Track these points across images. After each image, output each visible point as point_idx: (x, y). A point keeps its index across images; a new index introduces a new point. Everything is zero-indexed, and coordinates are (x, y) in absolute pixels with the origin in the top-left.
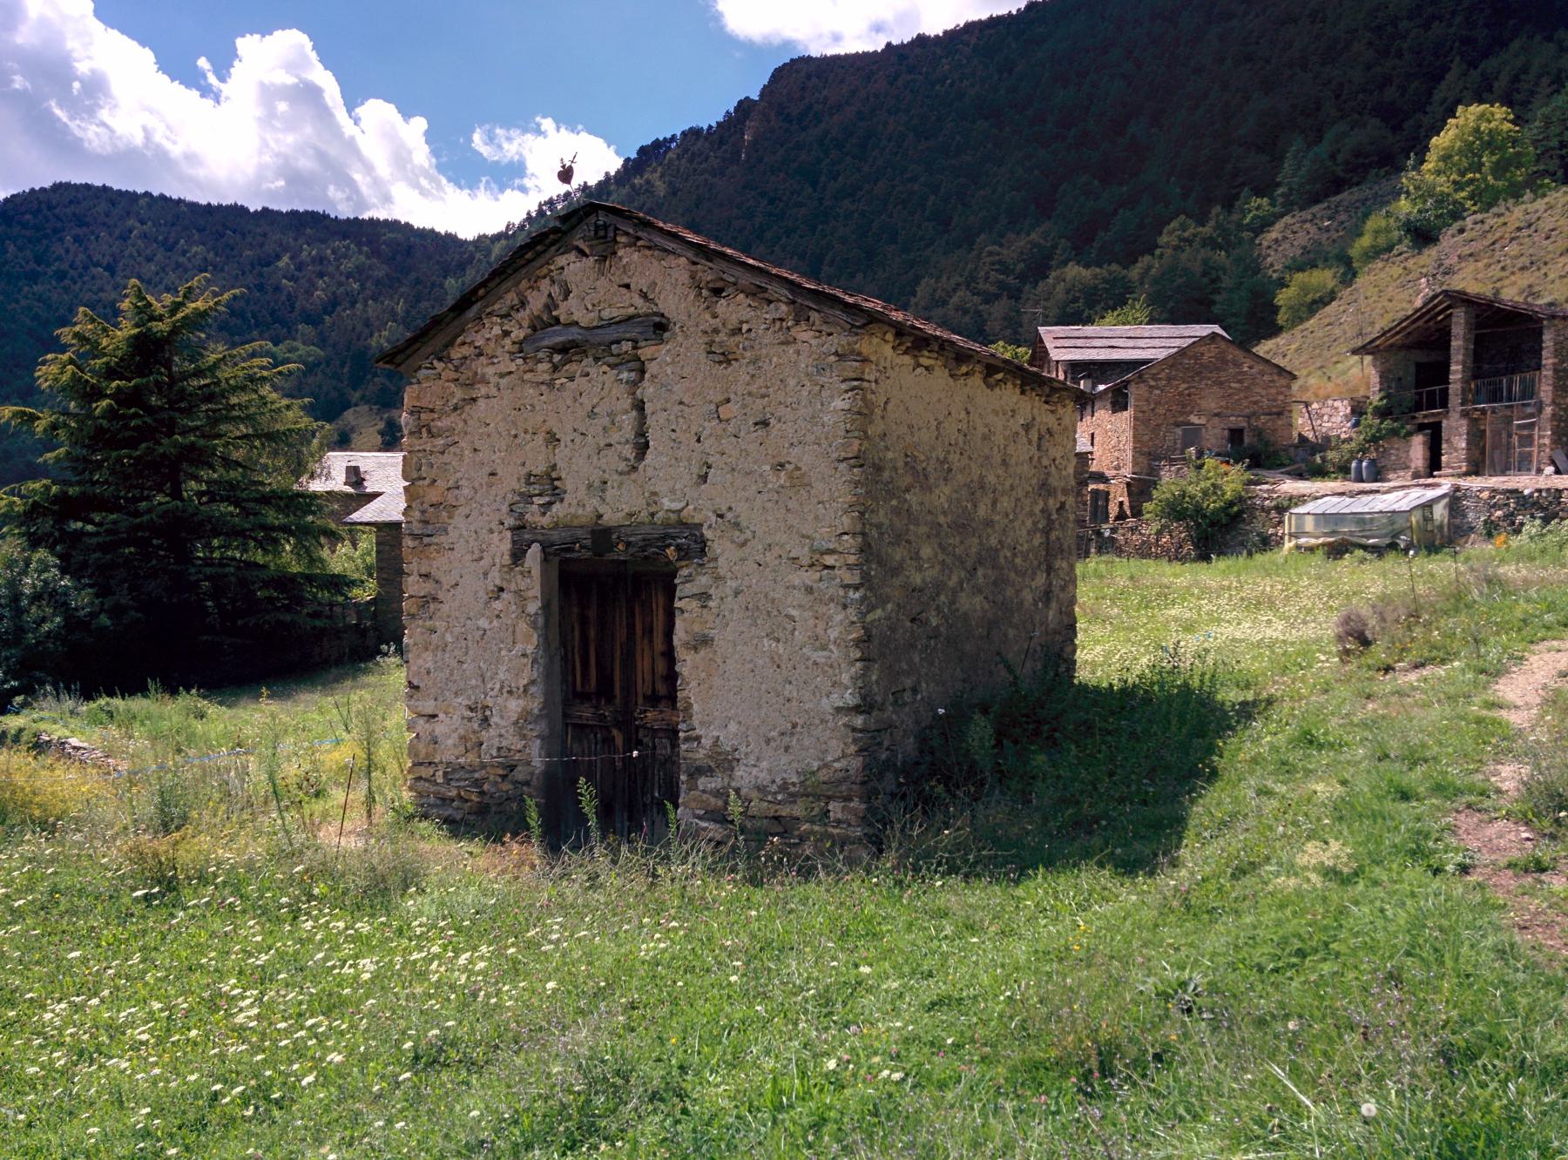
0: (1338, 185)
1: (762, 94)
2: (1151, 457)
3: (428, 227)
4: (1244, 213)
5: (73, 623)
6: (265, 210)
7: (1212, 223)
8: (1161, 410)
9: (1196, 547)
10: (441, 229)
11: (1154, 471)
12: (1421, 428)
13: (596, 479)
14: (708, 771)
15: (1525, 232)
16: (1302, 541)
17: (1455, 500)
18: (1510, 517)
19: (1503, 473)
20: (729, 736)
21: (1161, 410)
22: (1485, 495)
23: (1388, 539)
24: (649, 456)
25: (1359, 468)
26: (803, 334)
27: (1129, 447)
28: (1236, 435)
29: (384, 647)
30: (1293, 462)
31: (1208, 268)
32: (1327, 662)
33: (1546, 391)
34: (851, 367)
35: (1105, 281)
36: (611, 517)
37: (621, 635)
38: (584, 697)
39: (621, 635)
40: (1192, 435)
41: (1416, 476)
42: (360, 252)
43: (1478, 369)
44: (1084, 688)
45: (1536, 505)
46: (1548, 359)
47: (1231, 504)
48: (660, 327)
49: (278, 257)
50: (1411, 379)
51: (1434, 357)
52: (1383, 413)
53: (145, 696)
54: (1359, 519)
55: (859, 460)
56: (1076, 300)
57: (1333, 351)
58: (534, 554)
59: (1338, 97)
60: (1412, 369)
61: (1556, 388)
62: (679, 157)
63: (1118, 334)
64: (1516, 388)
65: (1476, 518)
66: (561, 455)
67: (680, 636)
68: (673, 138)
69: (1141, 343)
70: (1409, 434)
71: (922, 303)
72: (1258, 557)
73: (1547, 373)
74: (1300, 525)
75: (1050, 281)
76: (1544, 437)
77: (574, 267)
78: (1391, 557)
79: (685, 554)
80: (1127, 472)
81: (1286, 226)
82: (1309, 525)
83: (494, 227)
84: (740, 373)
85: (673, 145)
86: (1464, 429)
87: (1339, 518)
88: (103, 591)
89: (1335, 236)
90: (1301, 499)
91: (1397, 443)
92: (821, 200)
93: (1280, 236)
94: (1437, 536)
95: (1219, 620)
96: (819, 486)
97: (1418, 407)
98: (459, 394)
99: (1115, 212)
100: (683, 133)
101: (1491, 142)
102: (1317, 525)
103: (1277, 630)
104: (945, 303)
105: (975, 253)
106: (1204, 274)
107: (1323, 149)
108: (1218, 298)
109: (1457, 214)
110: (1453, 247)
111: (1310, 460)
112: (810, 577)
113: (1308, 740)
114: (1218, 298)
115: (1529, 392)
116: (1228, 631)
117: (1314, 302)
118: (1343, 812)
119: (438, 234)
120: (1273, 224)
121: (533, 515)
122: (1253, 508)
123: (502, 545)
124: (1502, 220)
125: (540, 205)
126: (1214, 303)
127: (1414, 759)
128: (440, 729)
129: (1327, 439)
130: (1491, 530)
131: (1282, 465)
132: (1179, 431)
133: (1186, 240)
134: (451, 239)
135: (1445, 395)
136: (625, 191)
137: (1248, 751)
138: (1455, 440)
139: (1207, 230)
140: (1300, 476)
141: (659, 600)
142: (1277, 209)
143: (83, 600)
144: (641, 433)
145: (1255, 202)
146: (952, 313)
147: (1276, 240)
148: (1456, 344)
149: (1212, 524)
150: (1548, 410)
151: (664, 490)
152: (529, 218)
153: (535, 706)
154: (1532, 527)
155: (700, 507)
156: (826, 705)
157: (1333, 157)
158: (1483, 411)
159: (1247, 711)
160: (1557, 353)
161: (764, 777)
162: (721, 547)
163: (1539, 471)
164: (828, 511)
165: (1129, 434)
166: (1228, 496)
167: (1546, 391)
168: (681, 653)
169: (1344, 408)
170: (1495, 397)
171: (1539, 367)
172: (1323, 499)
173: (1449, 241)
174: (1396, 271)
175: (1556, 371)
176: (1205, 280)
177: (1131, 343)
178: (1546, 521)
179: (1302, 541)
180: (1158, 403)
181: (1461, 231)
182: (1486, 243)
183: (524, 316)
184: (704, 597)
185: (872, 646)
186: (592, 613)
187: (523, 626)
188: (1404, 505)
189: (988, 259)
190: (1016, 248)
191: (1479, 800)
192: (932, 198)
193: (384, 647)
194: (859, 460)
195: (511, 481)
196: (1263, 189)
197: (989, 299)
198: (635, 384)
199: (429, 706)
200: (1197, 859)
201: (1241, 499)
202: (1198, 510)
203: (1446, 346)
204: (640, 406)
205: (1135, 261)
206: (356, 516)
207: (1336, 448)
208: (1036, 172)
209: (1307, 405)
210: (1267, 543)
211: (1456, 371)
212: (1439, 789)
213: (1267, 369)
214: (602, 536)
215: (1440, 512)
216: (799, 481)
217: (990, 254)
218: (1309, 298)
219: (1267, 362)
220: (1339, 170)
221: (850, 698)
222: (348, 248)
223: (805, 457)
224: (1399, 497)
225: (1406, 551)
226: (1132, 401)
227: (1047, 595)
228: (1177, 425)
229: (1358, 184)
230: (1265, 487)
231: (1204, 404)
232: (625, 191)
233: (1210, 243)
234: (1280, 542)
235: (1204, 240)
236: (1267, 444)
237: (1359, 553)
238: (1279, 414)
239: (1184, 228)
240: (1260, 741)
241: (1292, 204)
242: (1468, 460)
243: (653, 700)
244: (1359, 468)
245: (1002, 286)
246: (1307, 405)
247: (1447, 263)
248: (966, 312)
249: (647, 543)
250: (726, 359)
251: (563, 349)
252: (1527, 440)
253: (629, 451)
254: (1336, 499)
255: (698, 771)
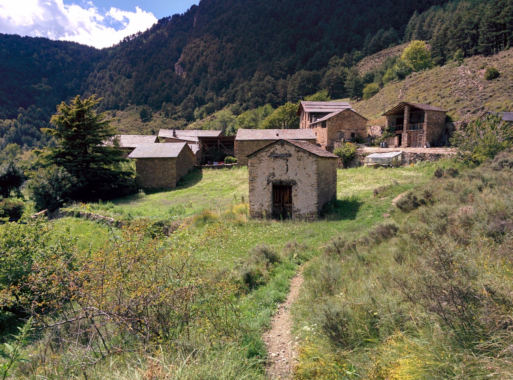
0: (380, 48)
1: (200, 4)
2: (332, 140)
3: (85, 44)
4: (353, 55)
5: (73, 185)
6: (26, 36)
7: (344, 58)
8: (334, 128)
9: (344, 164)
10: (89, 45)
11: (332, 144)
12: (397, 135)
13: (281, 174)
14: (296, 212)
15: (426, 80)
16: (369, 164)
17: (403, 155)
18: (414, 159)
19: (415, 147)
20: (299, 207)
21: (334, 128)
22: (409, 154)
23: (389, 164)
24: (288, 172)
25: (382, 144)
26: (310, 158)
27: (326, 137)
28: (353, 135)
29: (139, 190)
30: (367, 142)
31: (343, 73)
32: (372, 196)
33: (425, 128)
34: (317, 162)
35: (312, 76)
36: (282, 179)
37: (282, 195)
38: (276, 203)
39: (282, 195)
40: (342, 135)
41: (396, 147)
42: (62, 53)
43: (410, 122)
44: (339, 201)
45: (420, 157)
46: (426, 120)
47: (352, 154)
48: (290, 155)
49: (33, 54)
50: (395, 122)
51: (400, 117)
52: (388, 131)
53: (98, 203)
54: (381, 159)
55: (317, 174)
56: (304, 81)
57: (377, 109)
58: (271, 184)
59: (381, 17)
60: (396, 119)
61: (427, 127)
62: (172, 24)
63: (322, 104)
64: (419, 126)
65: (407, 159)
66: (275, 171)
67: (293, 194)
68: (170, 17)
69: (328, 107)
70: (394, 136)
71: (256, 79)
72: (359, 168)
73: (425, 123)
74: (368, 160)
75: (296, 74)
76: (424, 139)
77: (278, 147)
78: (388, 169)
79: (293, 184)
80: (326, 144)
81: (366, 60)
82: (370, 160)
83: (109, 44)
84: (302, 162)
85: (170, 20)
86: (407, 136)
87: (377, 159)
88: (78, 177)
89: (379, 64)
90: (368, 154)
91: (391, 138)
92: (221, 43)
93: (364, 63)
94: (397, 164)
95: (351, 185)
96: (312, 177)
97: (396, 130)
98: (258, 162)
99: (315, 52)
100: (173, 16)
101: (419, 51)
102: (372, 160)
103: (363, 188)
104: (263, 80)
105: (272, 63)
106: (342, 75)
107: (376, 37)
108: (346, 82)
109: (410, 71)
110: (409, 82)
111: (371, 141)
112: (311, 188)
113: (369, 207)
114: (346, 82)
115: (421, 128)
116: (353, 188)
117: (373, 92)
118: (372, 213)
119: (88, 47)
120: (361, 59)
121: (271, 178)
122: (357, 155)
123: (266, 182)
124: (420, 75)
125: (124, 38)
126: (344, 84)
127: (380, 208)
128: (255, 207)
129: (375, 136)
130: (410, 162)
131: (364, 143)
132: (339, 134)
133: (336, 63)
134: (92, 49)
135: (403, 127)
136: (154, 35)
137: (363, 208)
138: (405, 138)
139: (342, 61)
140: (368, 146)
141: (288, 190)
142: (363, 54)
143: (75, 179)
144: (287, 169)
145: (357, 52)
146: (265, 83)
147: (363, 65)
148: (405, 115)
149: (347, 159)
150: (425, 132)
151: (291, 176)
152: (121, 43)
153: (271, 204)
154: (419, 162)
155: (296, 178)
156: (313, 203)
157: (379, 39)
158: (411, 132)
159: (362, 203)
160: (428, 119)
161: (304, 212)
162: (299, 184)
163: (423, 147)
164: (314, 179)
165: (326, 134)
166: (351, 152)
167: (425, 128)
168: (293, 197)
169: (379, 128)
170: (414, 129)
171: (423, 122)
172: (373, 153)
173: (407, 80)
174: (394, 86)
175: (427, 123)
176: (342, 77)
177: (325, 107)
178: (422, 160)
179: (369, 164)
180: (334, 126)
181: (411, 77)
182: (416, 82)
183: (270, 152)
184: (296, 190)
185: (319, 196)
186: (278, 191)
187: (269, 193)
188: (392, 156)
189: (276, 66)
190: (284, 62)
191: (386, 212)
192: (257, 44)
193: (139, 190)
194: (317, 174)
195: (267, 174)
196: (359, 48)
197: (277, 79)
198: (286, 162)
199: (253, 204)
200: (357, 218)
201: (354, 153)
202: (344, 155)
203: (403, 114)
204: (287, 165)
205: (321, 68)
206: (130, 156)
207: (377, 139)
208: (290, 37)
209: (370, 127)
210: (360, 164)
211: (405, 122)
212: (382, 211)
213: (361, 118)
214: (281, 182)
215: (400, 158)
216: (309, 176)
217: (277, 64)
218: (371, 92)
219: (361, 116)
220: (381, 44)
221: (316, 202)
222: (57, 51)
223: (310, 173)
224: (391, 153)
225: (391, 167)
226: (327, 126)
227: (334, 187)
228: (338, 132)
229: (386, 48)
230: (360, 149)
231: (345, 127)
232: (154, 35)
233: (343, 65)
234: (363, 164)
235: (342, 63)
236: (360, 137)
237: (381, 167)
238: (364, 129)
239: (336, 59)
240: (364, 207)
241: (368, 53)
242: (407, 143)
243: (287, 203)
244: (382, 144)
245: (281, 74)
246: (370, 127)
247: (406, 86)
248: (270, 83)
249: (288, 183)
250: (300, 160)
251: (276, 157)
252: (420, 139)
253: (286, 171)
254: (377, 154)
255: (295, 212)
